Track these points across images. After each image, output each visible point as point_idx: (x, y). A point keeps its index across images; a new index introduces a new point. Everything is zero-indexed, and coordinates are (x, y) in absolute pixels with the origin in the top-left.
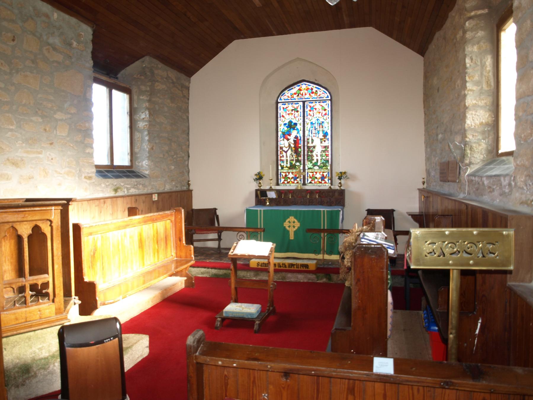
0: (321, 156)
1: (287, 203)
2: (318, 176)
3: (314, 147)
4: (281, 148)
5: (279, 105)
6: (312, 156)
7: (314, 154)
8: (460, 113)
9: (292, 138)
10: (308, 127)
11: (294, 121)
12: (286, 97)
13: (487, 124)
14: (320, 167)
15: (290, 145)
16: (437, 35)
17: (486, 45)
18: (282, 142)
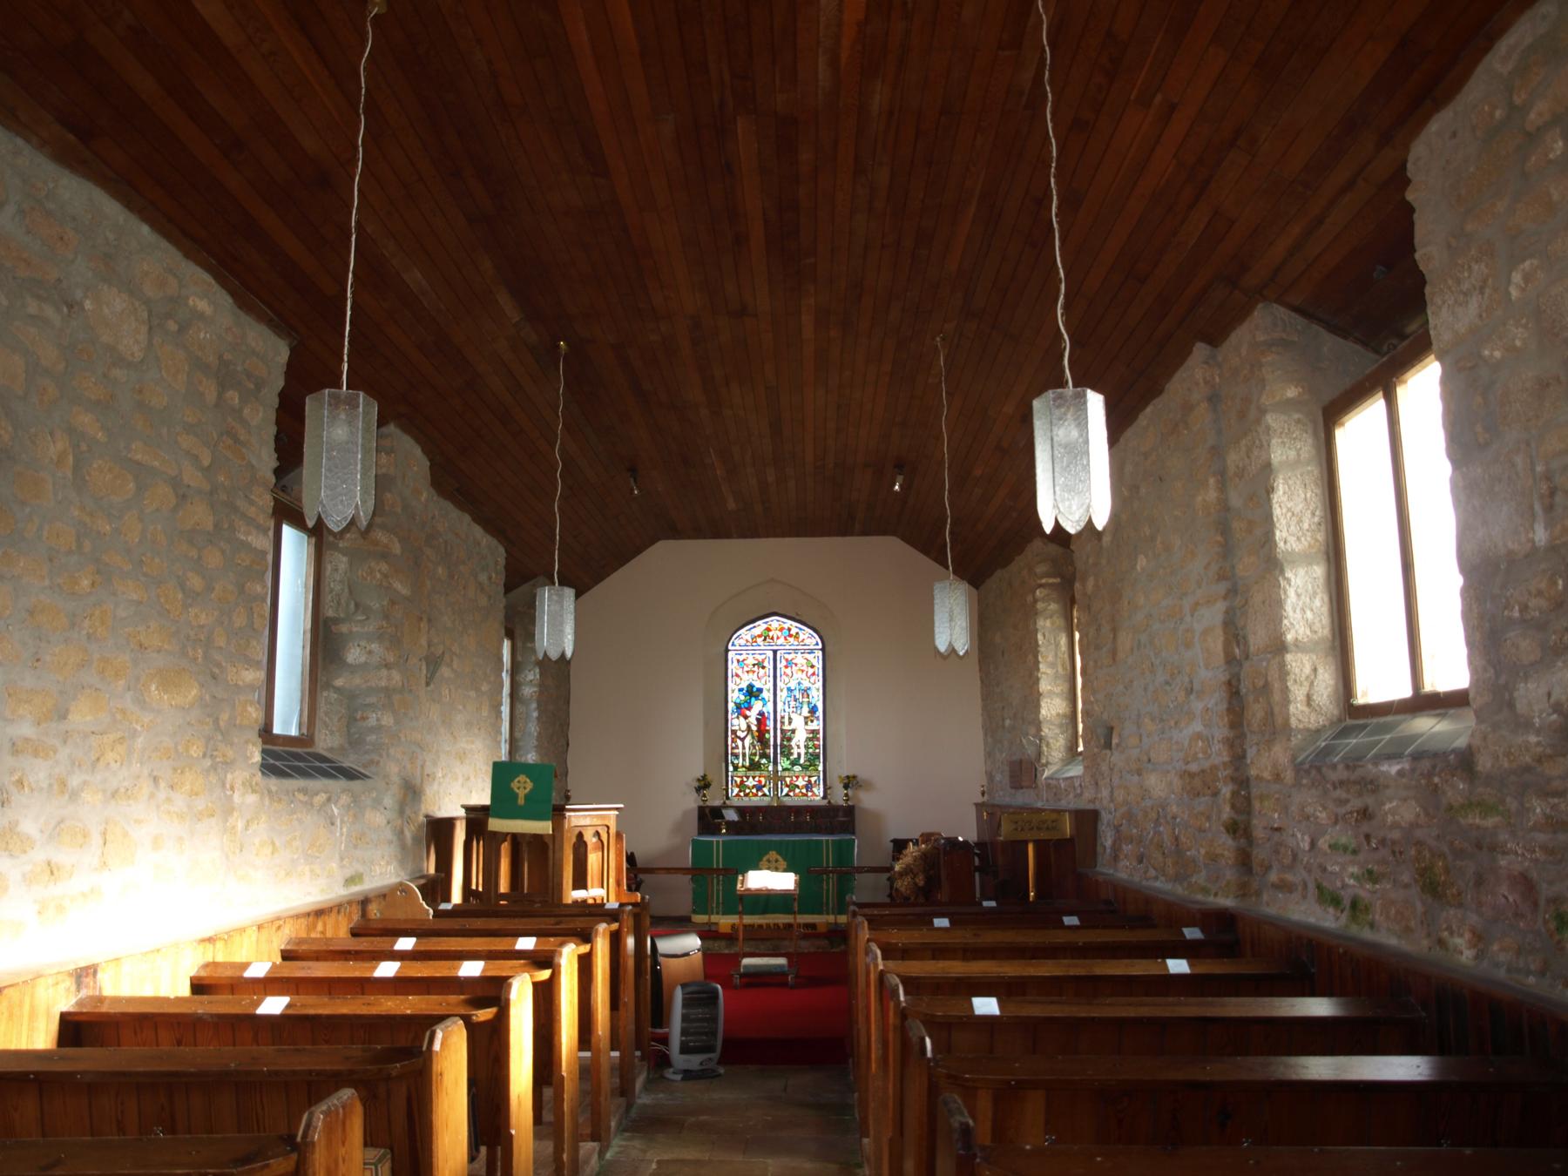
0: (806, 747)
1: (754, 829)
2: (801, 782)
3: (793, 731)
4: (734, 732)
5: (731, 655)
6: (790, 747)
7: (793, 743)
8: (1032, 699)
9: (753, 715)
10: (782, 695)
11: (758, 685)
12: (742, 642)
13: (1065, 716)
14: (805, 768)
15: (749, 727)
16: (998, 573)
17: (1060, 622)
18: (735, 722)
